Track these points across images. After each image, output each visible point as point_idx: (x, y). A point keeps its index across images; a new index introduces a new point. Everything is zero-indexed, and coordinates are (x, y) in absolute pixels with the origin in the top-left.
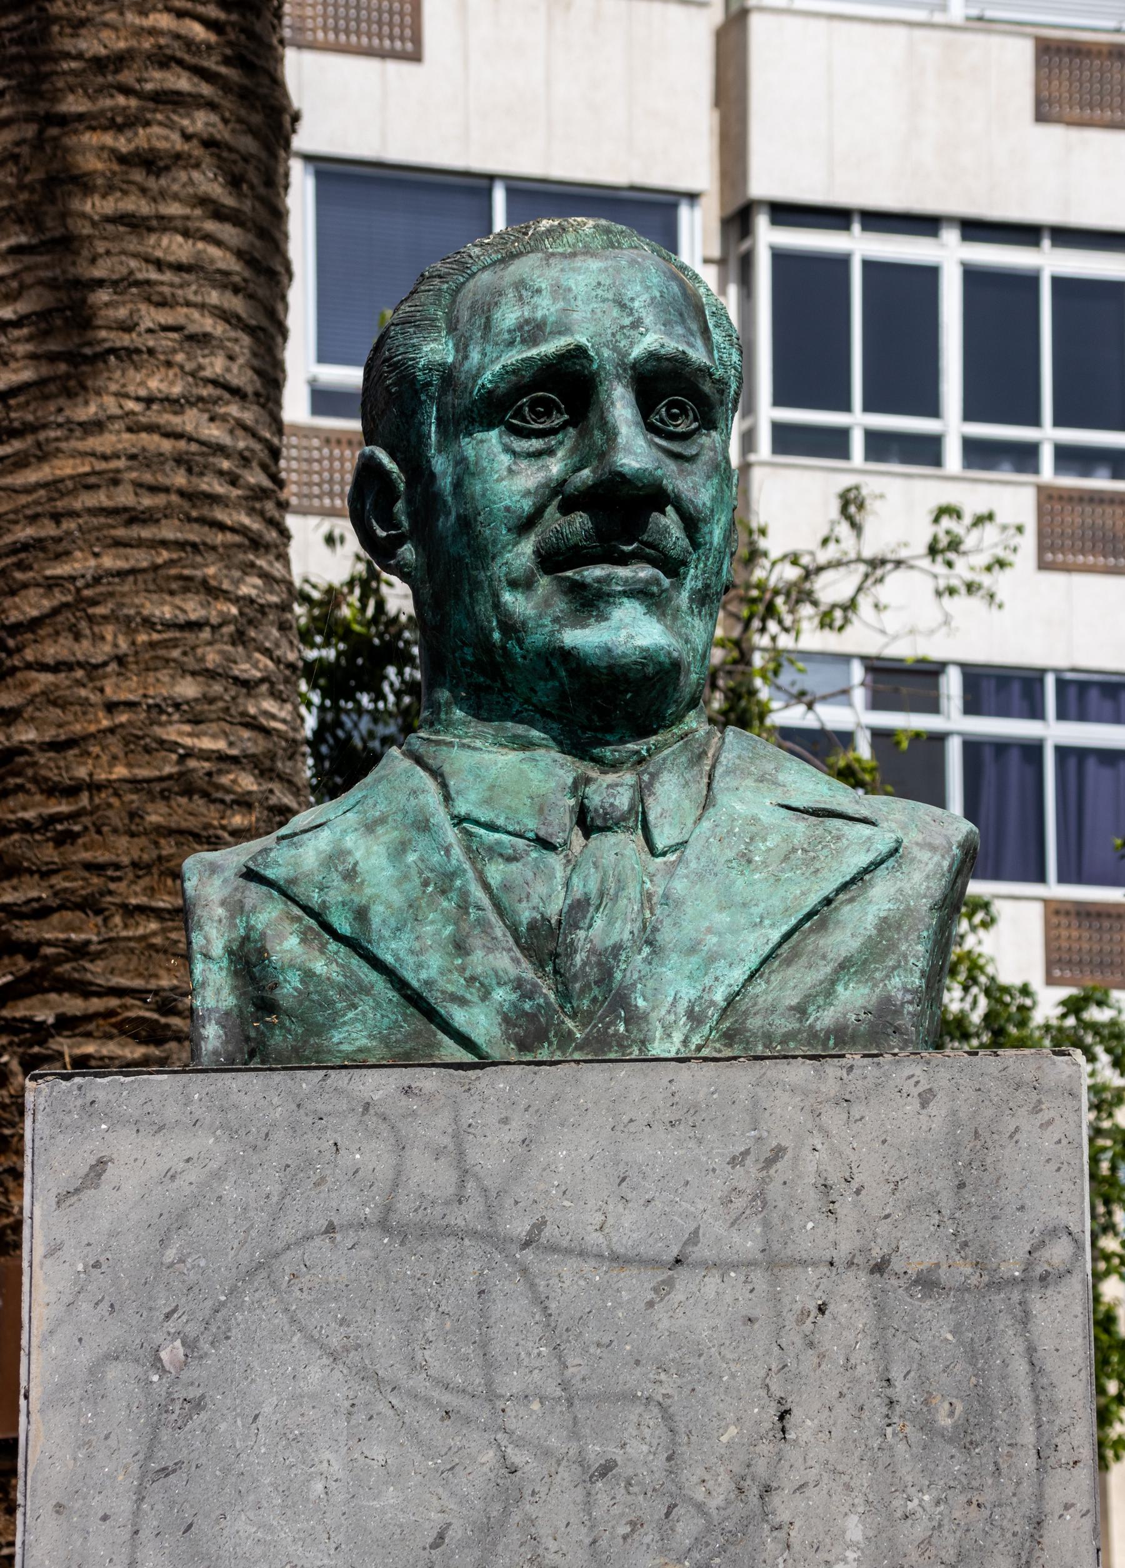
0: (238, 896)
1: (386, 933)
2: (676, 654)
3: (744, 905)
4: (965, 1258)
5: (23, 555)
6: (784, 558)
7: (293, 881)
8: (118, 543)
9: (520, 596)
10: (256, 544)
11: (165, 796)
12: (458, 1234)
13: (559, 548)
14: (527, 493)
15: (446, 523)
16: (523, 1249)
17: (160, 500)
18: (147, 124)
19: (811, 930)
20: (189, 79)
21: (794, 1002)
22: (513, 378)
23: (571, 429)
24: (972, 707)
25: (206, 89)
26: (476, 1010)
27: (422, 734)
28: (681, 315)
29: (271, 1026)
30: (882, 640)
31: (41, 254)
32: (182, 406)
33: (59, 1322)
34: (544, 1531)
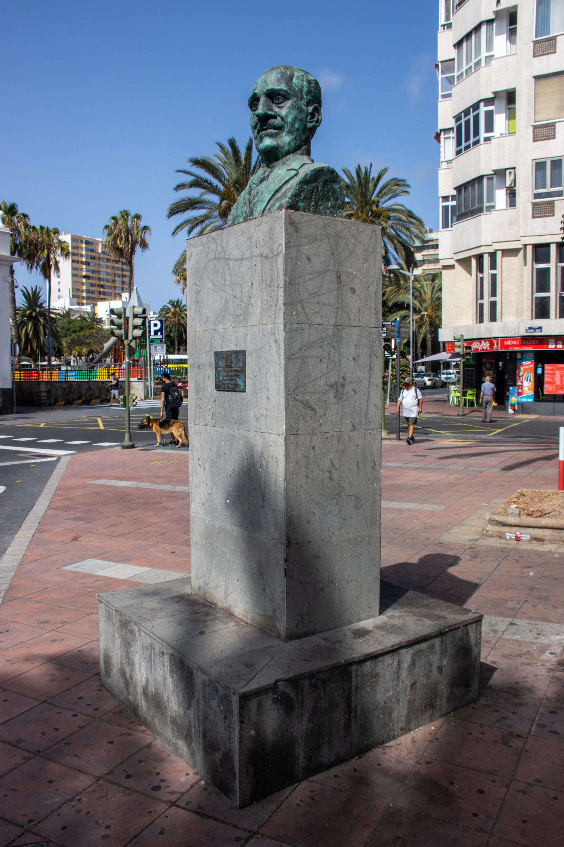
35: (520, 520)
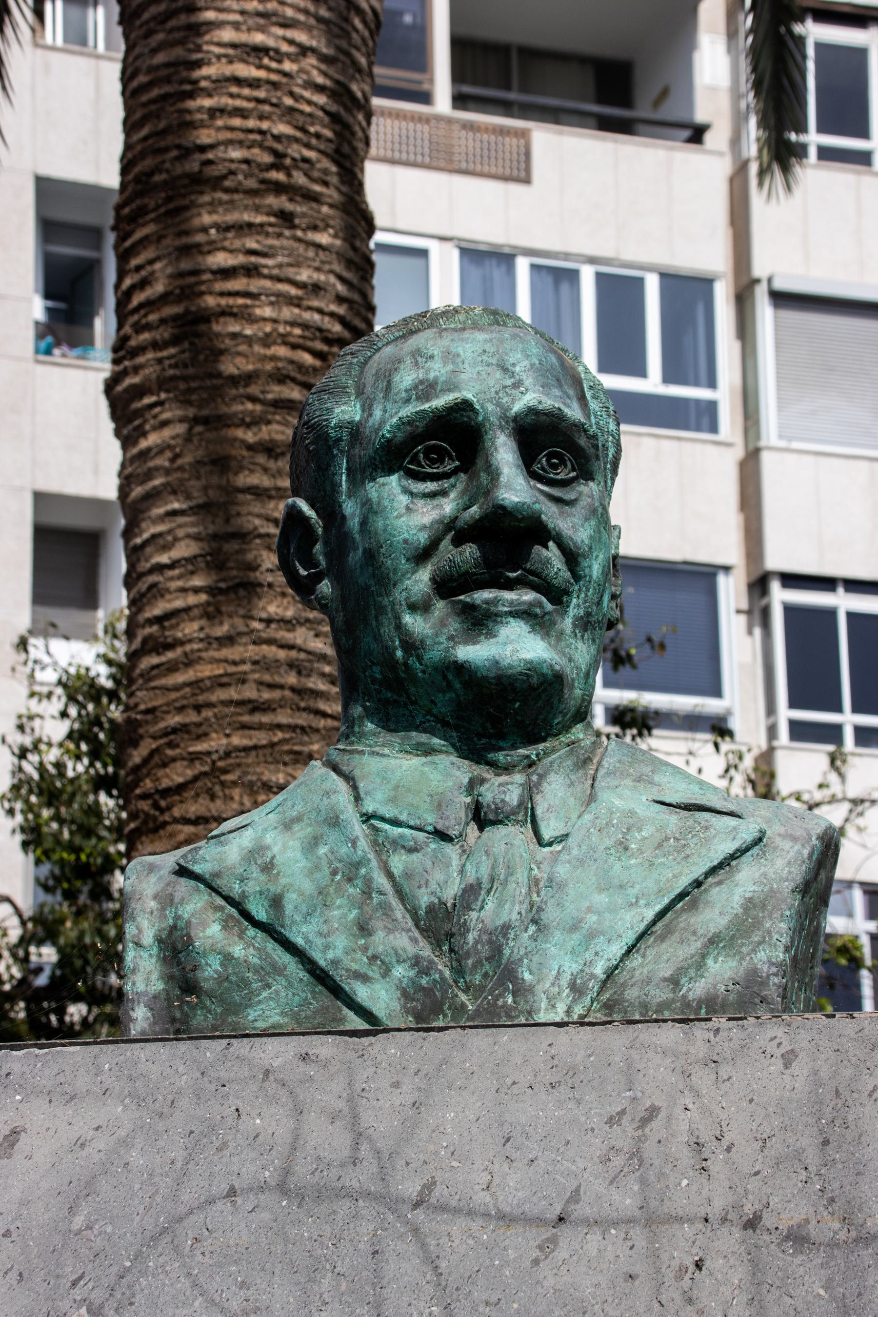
0: (170, 890)
1: (298, 918)
2: (557, 667)
3: (621, 886)
4: (832, 1214)
5: (172, 737)
6: (791, 795)
7: (217, 875)
8: (244, 727)
9: (418, 618)
12: (353, 1196)
13: (452, 576)
14: (423, 528)
15: (355, 557)
16: (414, 1209)
17: (277, 694)
18: (269, 423)
19: (683, 909)
20: (300, 391)
21: (668, 974)
22: (408, 428)
23: (462, 475)
26: (377, 986)
27: (339, 746)
28: (558, 380)
29: (193, 1007)
31: (189, 515)
32: (294, 625)
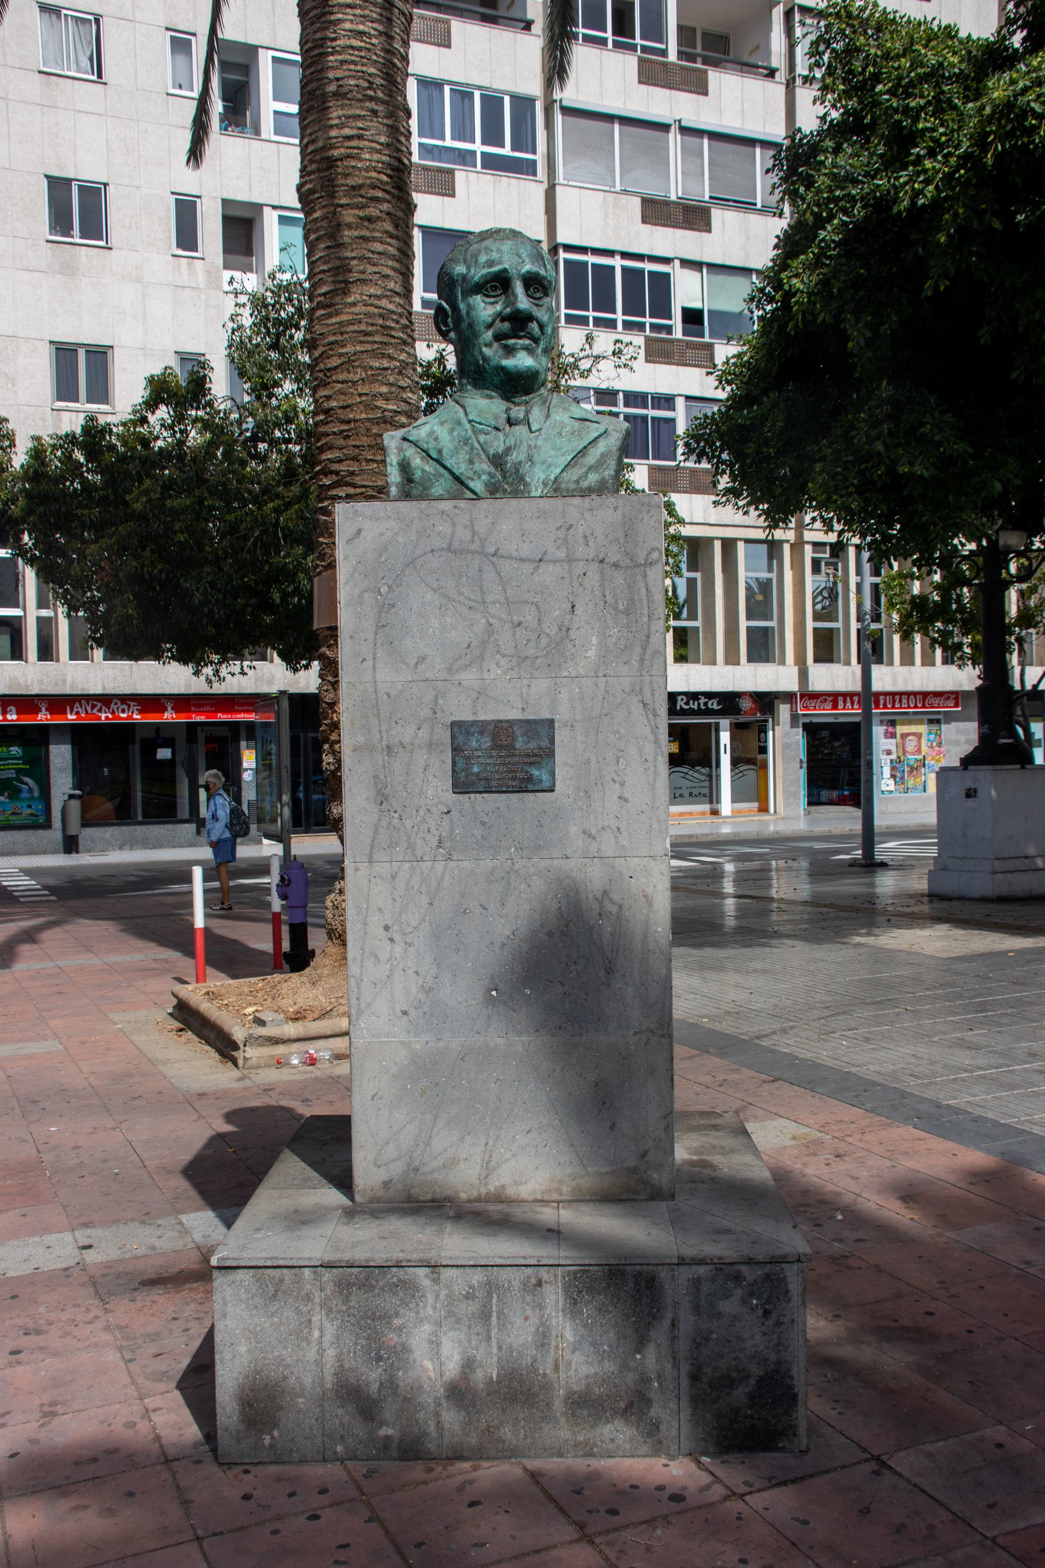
8: (361, 342)
10: (405, 343)
11: (378, 424)
12: (472, 553)
17: (374, 328)
24: (626, 405)
25: (387, 196)
30: (599, 382)
33: (349, 580)
34: (501, 643)
35: (305, 1027)
